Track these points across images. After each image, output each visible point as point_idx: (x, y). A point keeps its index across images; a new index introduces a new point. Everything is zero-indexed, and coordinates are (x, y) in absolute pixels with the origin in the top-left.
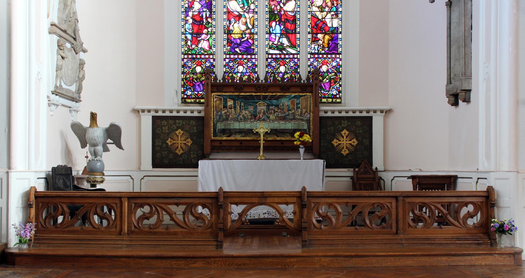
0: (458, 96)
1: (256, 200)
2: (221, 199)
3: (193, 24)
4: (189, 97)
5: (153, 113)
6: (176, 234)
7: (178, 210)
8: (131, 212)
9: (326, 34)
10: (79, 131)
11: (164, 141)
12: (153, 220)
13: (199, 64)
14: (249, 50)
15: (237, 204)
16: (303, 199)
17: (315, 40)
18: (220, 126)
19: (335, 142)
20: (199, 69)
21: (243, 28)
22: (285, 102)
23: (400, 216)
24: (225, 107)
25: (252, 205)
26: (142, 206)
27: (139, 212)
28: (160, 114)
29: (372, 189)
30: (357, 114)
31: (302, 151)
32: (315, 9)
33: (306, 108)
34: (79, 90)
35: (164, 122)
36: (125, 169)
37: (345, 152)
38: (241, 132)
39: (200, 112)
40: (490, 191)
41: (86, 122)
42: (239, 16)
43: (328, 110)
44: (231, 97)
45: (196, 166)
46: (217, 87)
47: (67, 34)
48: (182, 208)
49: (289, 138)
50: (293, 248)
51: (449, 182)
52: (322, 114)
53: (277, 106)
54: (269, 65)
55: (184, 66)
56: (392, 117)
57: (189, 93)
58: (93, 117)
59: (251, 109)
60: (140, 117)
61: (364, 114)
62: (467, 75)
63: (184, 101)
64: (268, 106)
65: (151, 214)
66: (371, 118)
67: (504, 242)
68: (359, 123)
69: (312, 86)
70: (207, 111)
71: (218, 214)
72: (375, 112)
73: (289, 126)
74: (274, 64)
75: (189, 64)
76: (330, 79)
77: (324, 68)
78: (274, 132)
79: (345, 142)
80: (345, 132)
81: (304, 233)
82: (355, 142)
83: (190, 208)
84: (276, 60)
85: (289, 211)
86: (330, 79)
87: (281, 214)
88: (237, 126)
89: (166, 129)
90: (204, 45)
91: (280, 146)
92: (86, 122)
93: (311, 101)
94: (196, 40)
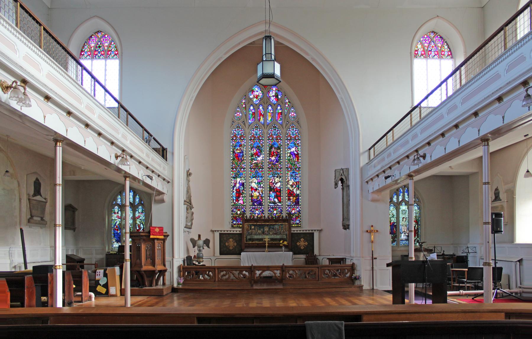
0: (346, 227)
1: (265, 269)
2: (253, 269)
3: (236, 193)
4: (235, 224)
5: (220, 232)
6: (235, 281)
7: (236, 273)
8: (218, 274)
9: (294, 197)
10: (194, 243)
11: (225, 244)
12: (227, 276)
13: (239, 210)
14: (260, 204)
15: (258, 270)
16: (283, 268)
17: (289, 199)
18: (248, 237)
19: (298, 244)
20: (239, 212)
21: (258, 194)
22: (276, 227)
23: (320, 274)
24: (251, 229)
25: (264, 271)
26: (223, 271)
27: (222, 273)
28: (223, 232)
29: (314, 264)
30: (308, 232)
31: (283, 248)
32: (289, 186)
33: (285, 229)
34: (192, 224)
35: (224, 236)
36: (211, 257)
37: (302, 248)
38: (258, 240)
39: (240, 231)
40: (353, 264)
41: (196, 238)
42: (256, 190)
43: (294, 230)
44: (253, 225)
45: (240, 254)
46: (247, 221)
47: (189, 204)
48: (238, 272)
49: (278, 242)
50: (280, 287)
51: (341, 260)
52: (292, 232)
53: (273, 228)
54: (269, 210)
55: (232, 211)
56: (323, 234)
57: (235, 222)
58: (199, 236)
59: (262, 230)
60: (214, 234)
61: (311, 232)
62: (348, 219)
63: (232, 227)
64: (269, 229)
65: (226, 274)
66: (313, 233)
67: (357, 283)
68: (308, 235)
69: (287, 220)
70: (243, 230)
71: (251, 274)
72: (315, 230)
73: (278, 237)
74: (271, 210)
75: (235, 210)
76: (296, 216)
77: (293, 212)
78: (272, 239)
79: (302, 243)
80: (302, 239)
81: (284, 281)
82: (306, 243)
83: (241, 272)
84: (272, 208)
85: (278, 273)
86: (296, 216)
87: (275, 274)
88: (256, 237)
89: (225, 239)
90: (241, 202)
91: (274, 246)
92: (196, 238)
93: (287, 226)
94: (237, 200)
